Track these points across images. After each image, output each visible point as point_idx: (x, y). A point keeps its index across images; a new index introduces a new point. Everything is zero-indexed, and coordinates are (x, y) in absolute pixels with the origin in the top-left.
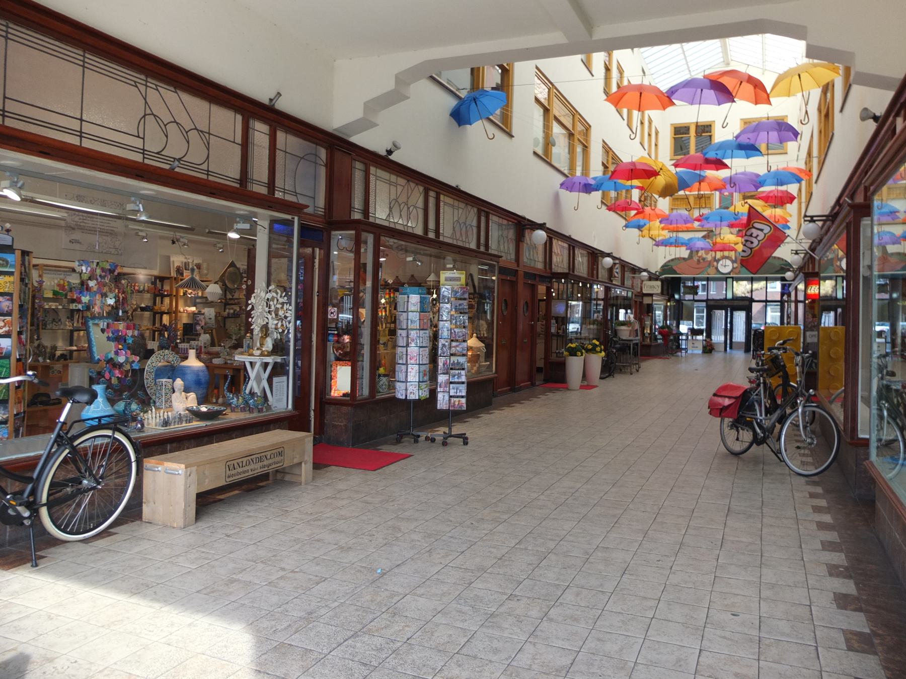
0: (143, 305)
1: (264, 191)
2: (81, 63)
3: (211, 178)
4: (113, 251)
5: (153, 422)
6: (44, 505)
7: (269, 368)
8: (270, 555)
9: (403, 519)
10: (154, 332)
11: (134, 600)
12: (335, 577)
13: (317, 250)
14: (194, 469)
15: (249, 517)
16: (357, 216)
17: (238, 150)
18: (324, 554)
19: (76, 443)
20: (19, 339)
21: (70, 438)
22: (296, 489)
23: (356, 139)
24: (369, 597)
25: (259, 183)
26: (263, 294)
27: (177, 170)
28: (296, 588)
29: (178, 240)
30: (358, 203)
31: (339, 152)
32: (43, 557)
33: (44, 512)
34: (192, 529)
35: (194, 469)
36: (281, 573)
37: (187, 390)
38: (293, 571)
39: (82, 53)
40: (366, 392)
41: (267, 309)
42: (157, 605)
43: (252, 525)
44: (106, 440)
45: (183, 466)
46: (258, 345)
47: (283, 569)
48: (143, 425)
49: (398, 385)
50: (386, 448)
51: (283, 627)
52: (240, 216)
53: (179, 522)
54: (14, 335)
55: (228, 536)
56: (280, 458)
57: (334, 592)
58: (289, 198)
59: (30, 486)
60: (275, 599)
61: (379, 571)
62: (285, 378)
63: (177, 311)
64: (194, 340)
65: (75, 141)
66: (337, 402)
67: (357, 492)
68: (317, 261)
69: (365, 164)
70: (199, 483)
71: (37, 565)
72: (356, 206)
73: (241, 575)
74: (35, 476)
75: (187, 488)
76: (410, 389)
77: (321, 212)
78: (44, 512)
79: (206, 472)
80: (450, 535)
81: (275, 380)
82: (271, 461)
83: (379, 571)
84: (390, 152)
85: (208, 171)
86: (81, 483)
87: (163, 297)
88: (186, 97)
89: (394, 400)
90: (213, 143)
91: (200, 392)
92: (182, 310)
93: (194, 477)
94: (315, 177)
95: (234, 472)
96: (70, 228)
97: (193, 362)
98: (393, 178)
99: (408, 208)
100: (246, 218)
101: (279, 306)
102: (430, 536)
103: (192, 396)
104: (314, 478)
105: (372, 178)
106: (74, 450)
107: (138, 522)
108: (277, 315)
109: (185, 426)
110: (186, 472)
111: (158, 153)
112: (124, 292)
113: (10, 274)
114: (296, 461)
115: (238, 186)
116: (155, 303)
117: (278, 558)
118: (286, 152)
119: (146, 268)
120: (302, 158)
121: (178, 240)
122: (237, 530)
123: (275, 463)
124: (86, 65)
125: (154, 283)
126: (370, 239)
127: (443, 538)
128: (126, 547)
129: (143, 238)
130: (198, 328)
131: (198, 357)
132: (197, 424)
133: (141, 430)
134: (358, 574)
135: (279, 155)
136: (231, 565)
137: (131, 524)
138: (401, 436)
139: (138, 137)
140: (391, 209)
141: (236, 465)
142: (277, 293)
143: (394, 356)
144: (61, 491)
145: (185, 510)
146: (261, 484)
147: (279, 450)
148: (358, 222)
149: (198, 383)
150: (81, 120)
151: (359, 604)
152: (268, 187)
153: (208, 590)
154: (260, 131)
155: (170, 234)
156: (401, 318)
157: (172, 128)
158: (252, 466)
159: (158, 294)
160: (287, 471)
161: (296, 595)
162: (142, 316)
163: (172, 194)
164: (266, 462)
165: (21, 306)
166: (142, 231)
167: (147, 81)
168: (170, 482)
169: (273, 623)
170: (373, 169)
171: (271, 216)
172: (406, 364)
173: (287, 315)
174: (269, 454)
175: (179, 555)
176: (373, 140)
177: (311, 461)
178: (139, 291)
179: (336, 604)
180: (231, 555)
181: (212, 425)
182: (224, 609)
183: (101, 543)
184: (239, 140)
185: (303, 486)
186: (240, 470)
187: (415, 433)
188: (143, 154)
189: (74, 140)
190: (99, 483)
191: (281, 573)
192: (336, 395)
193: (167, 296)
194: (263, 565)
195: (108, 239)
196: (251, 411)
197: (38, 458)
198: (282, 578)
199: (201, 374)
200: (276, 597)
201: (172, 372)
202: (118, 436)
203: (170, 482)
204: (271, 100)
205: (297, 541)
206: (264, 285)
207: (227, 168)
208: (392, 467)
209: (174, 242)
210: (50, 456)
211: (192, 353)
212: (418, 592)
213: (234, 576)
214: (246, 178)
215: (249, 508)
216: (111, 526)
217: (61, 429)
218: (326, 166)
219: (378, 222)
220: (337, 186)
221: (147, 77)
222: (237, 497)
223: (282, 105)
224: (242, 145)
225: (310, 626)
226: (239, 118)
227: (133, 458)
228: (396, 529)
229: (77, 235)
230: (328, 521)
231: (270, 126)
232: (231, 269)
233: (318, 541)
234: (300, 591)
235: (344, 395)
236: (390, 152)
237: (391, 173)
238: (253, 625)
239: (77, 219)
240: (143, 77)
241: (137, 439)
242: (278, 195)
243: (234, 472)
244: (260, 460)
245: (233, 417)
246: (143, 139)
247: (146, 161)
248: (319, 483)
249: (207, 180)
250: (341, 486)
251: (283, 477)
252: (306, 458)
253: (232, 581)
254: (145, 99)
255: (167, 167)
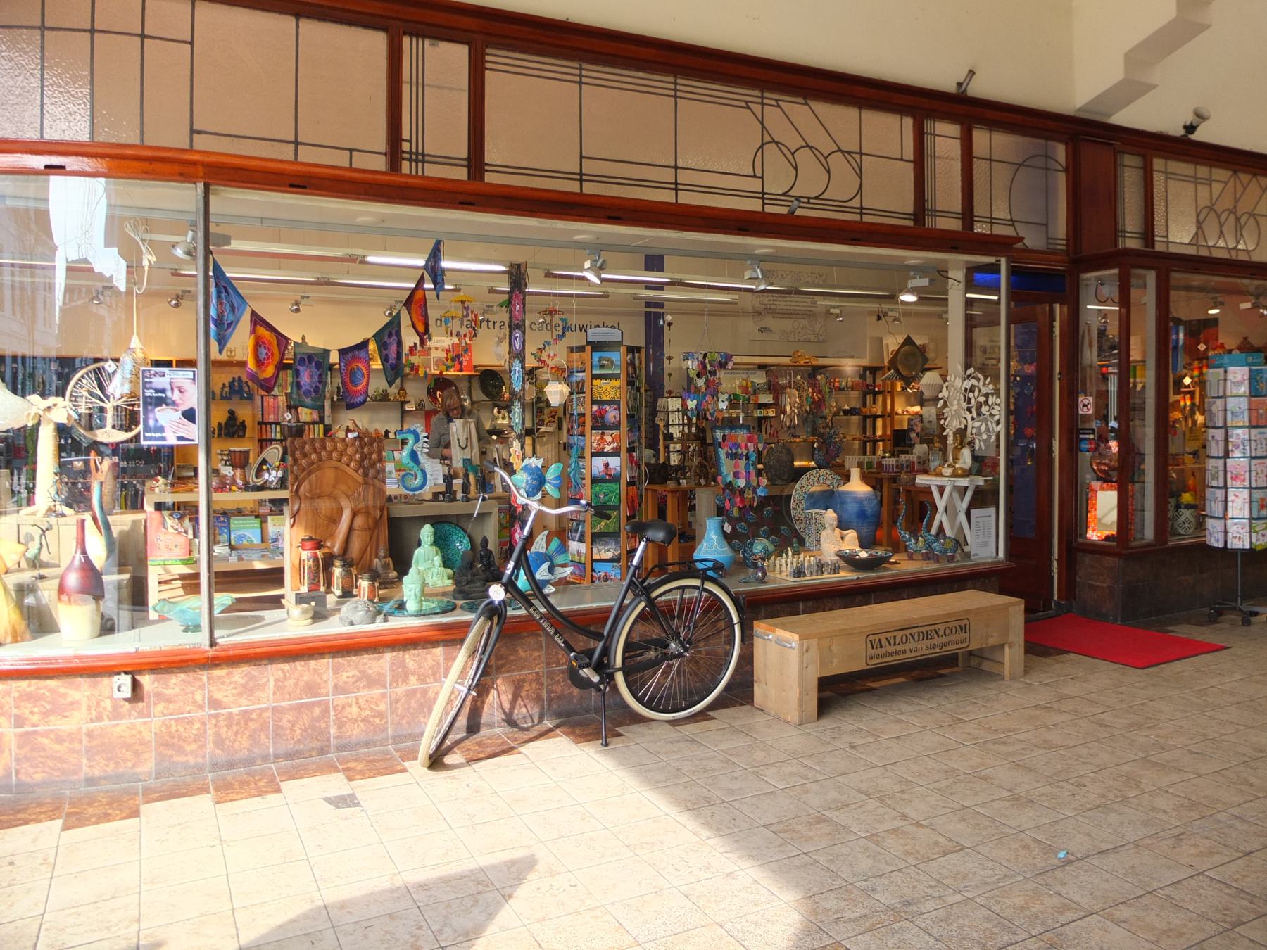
0: (847, 408)
1: (954, 225)
2: (673, 93)
3: (866, 219)
4: (812, 338)
5: (783, 571)
6: (618, 670)
7: (969, 495)
8: (897, 788)
9: (1154, 764)
10: (865, 443)
11: (684, 818)
12: (979, 848)
13: (1057, 307)
14: (815, 641)
15: (898, 721)
16: (1131, 243)
17: (908, 170)
18: (982, 805)
19: (654, 594)
20: (631, 457)
21: (645, 588)
22: (993, 685)
23: (1122, 118)
24: (1019, 901)
25: (948, 214)
26: (958, 382)
27: (799, 212)
28: (908, 853)
29: (885, 314)
30: (1131, 221)
31: (1090, 147)
32: (620, 735)
33: (619, 678)
34: (812, 728)
35: (815, 641)
36: (898, 823)
37: (842, 525)
38: (918, 824)
39: (759, 94)
40: (1149, 533)
41: (965, 405)
42: (705, 833)
43: (900, 734)
44: (696, 594)
45: (796, 637)
46: (951, 459)
47: (904, 816)
48: (764, 574)
49: (1210, 523)
50: (1183, 631)
51: (852, 916)
52: (914, 268)
53: (793, 716)
54: (624, 452)
55: (852, 747)
56: (961, 636)
57: (965, 876)
58: (999, 230)
59: (601, 644)
60: (865, 864)
61: (1061, 855)
62: (993, 510)
63: (892, 414)
64: (907, 453)
65: (573, 187)
66: (1095, 549)
67: (1092, 703)
68: (1057, 324)
69: (1144, 156)
70: (823, 663)
71: (607, 745)
72: (1128, 228)
73: (837, 813)
74: (605, 633)
75: (803, 668)
76: (1233, 530)
77: (1061, 245)
78: (619, 678)
79: (834, 648)
80: (1236, 811)
81: (973, 511)
82: (944, 639)
83: (1061, 855)
84: (1191, 128)
85: (862, 208)
86: (667, 646)
87: (875, 394)
88: (821, 108)
89: (1205, 548)
90: (873, 164)
91: (865, 530)
92: (900, 411)
93: (814, 651)
94: (1048, 193)
95: (880, 651)
96: (757, 313)
97: (857, 487)
98: (1203, 171)
99: (1238, 219)
100: (921, 270)
101: (982, 399)
102: (1194, 806)
103: (851, 534)
104: (1027, 671)
105: (1158, 178)
106: (651, 602)
107: (749, 707)
108: (979, 414)
109: (827, 577)
110: (801, 646)
111: (784, 194)
112: (820, 392)
113: (616, 377)
114: (992, 642)
115: (911, 223)
116: (865, 405)
117: (906, 796)
118: (991, 160)
119: (852, 357)
120: (1020, 165)
121: (885, 314)
122: (871, 739)
123: (953, 643)
124: (679, 94)
125: (863, 376)
126: (1151, 277)
127: (1222, 816)
128: (719, 739)
129: (838, 316)
130: (913, 435)
131: (865, 478)
132: (845, 575)
133: (761, 581)
134: (1022, 853)
135: (979, 168)
136: (833, 794)
137: (739, 708)
138: (1220, 613)
139: (755, 176)
140: (1199, 225)
141: (884, 642)
142: (978, 380)
143: (1203, 471)
144: (641, 654)
145: (801, 700)
146: (942, 672)
147: (962, 624)
148: (1128, 252)
149: (862, 514)
150: (676, 167)
151: (996, 908)
152: (963, 219)
153: (781, 827)
154: (945, 138)
155: (874, 306)
156: (1214, 409)
157: (804, 157)
158: (913, 645)
159: (869, 391)
160: (987, 655)
161: (902, 865)
162: (848, 422)
163: (801, 249)
164: (936, 641)
165: (631, 417)
166: (834, 307)
167: (676, 84)
168: (785, 656)
169: (843, 904)
170: (1158, 163)
171: (967, 262)
172: (1225, 487)
173: (994, 412)
174: (942, 627)
175: (771, 765)
176: (1153, 114)
177: (1022, 643)
178: (840, 389)
179: (958, 898)
180: (840, 779)
181: (868, 578)
182: (787, 862)
183: (689, 729)
184: (909, 153)
185: (1007, 682)
186: (893, 649)
187: (1246, 607)
188: (763, 199)
189: (667, 197)
190: (686, 650)
191: (898, 823)
192: (1095, 538)
193: (879, 392)
194: (877, 804)
195: (805, 322)
196: (938, 560)
197: (609, 610)
198: (894, 831)
199: (865, 503)
200: (870, 861)
201: (827, 499)
202: (710, 586)
203: (785, 656)
204: (959, 85)
205: (950, 772)
206: (960, 368)
207: (890, 196)
208: (1178, 666)
209: (879, 318)
210: (622, 609)
211: (855, 473)
212: (1117, 914)
213: (827, 813)
214: (924, 210)
215: (904, 707)
216: (712, 707)
217: (634, 575)
218: (1066, 170)
219: (1173, 249)
220: (1091, 200)
221: (762, 91)
222: (898, 688)
223: (981, 88)
224: (914, 162)
225: (897, 926)
226: (908, 122)
227: (735, 619)
228: (1133, 781)
229: (769, 322)
230: (1018, 747)
231: (962, 124)
232: (907, 348)
233: (984, 778)
234: (911, 860)
235: (1108, 538)
236: (1191, 128)
237: (1196, 164)
238: (812, 897)
239: (766, 301)
240: (757, 93)
241: (737, 593)
242: (979, 228)
243: (880, 651)
244: (926, 636)
245: (904, 566)
246: (762, 178)
247: (768, 209)
248: (1034, 679)
249: (861, 222)
250: (1071, 689)
251: (979, 664)
252: (1012, 638)
253: (821, 820)
254: (762, 123)
255: (784, 211)
